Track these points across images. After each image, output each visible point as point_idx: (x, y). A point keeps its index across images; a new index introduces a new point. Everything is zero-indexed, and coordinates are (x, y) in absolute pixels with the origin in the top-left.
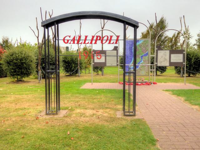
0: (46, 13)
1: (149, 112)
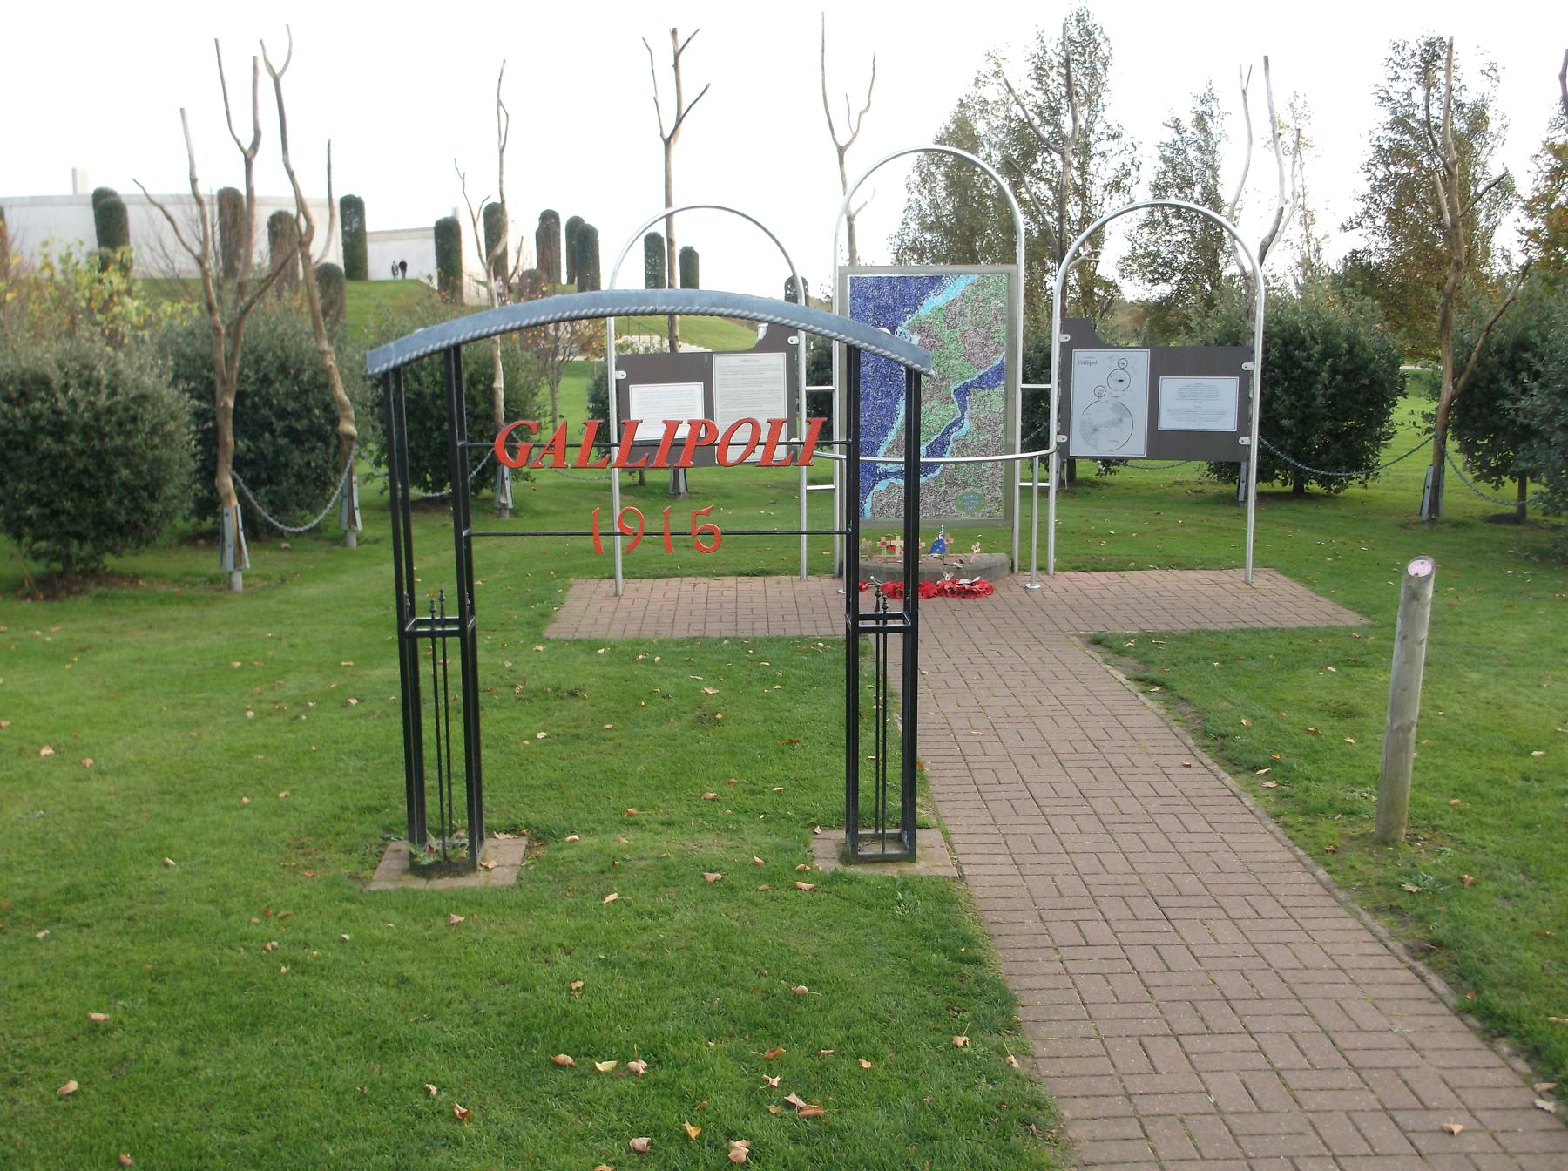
0: (255, 68)
1: (990, 829)
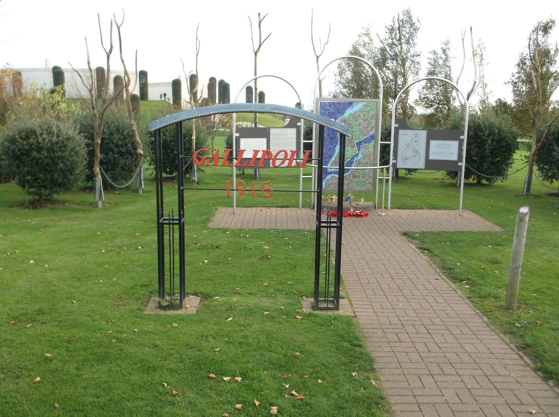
0: (111, 23)
